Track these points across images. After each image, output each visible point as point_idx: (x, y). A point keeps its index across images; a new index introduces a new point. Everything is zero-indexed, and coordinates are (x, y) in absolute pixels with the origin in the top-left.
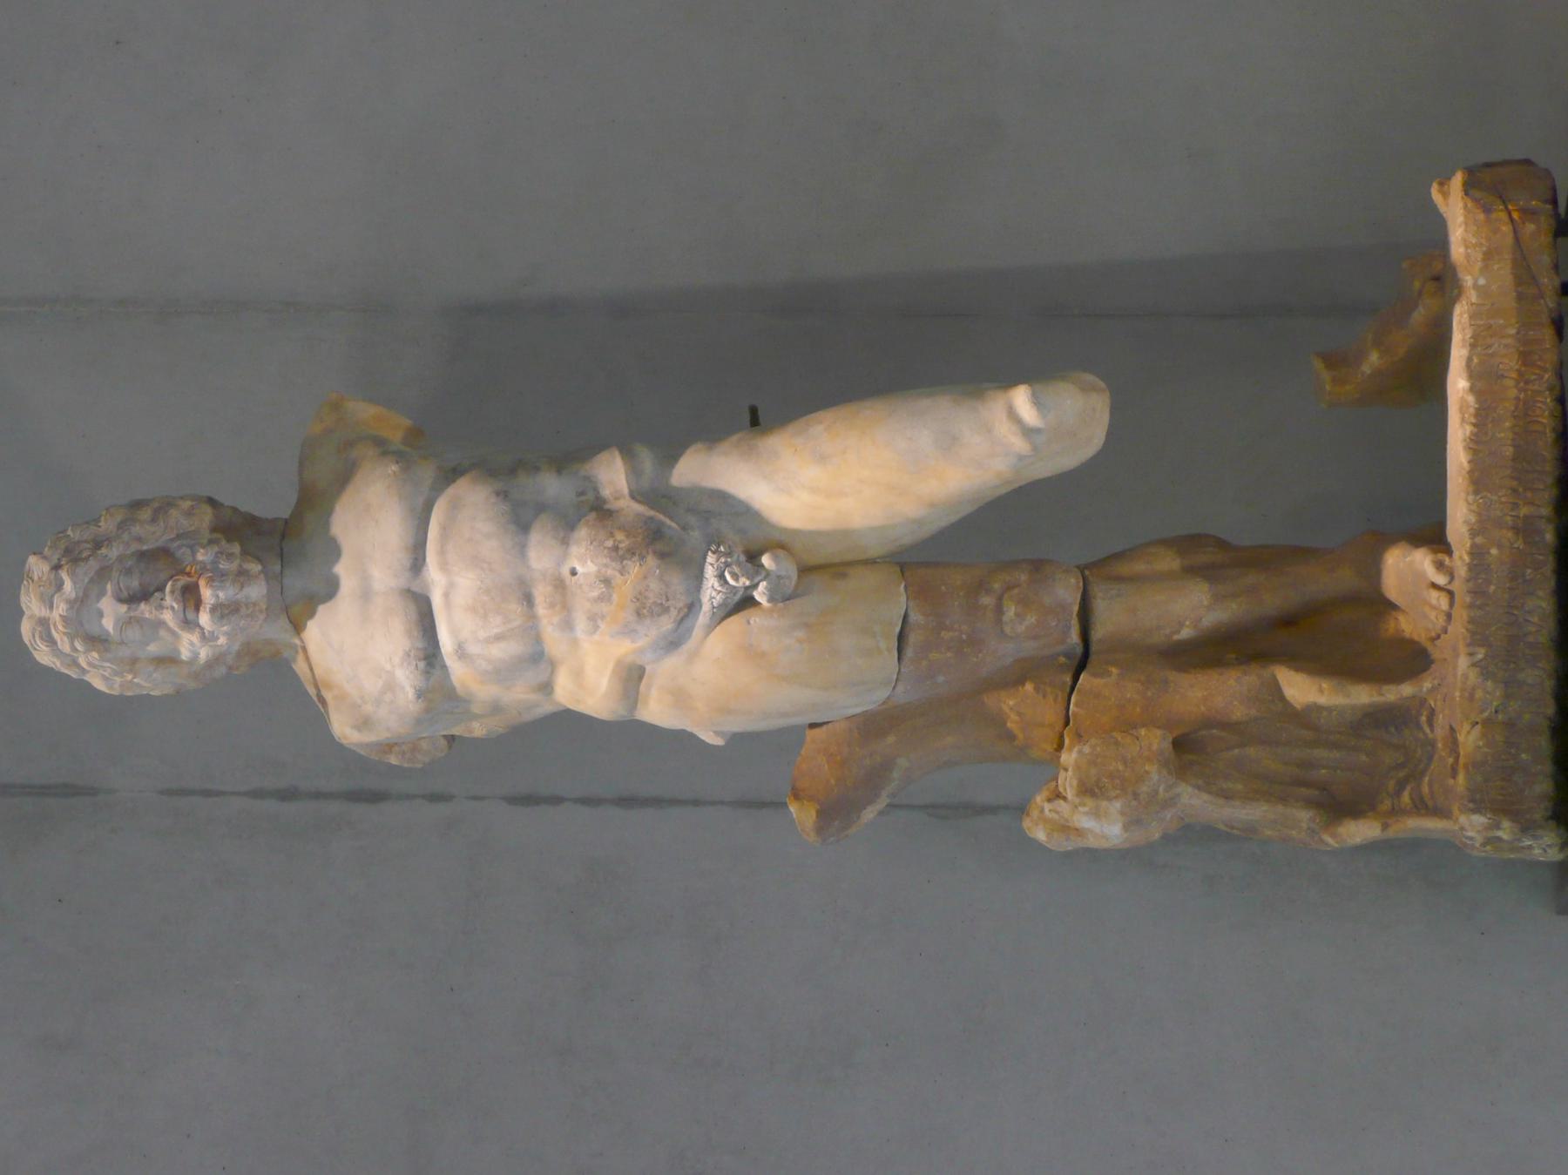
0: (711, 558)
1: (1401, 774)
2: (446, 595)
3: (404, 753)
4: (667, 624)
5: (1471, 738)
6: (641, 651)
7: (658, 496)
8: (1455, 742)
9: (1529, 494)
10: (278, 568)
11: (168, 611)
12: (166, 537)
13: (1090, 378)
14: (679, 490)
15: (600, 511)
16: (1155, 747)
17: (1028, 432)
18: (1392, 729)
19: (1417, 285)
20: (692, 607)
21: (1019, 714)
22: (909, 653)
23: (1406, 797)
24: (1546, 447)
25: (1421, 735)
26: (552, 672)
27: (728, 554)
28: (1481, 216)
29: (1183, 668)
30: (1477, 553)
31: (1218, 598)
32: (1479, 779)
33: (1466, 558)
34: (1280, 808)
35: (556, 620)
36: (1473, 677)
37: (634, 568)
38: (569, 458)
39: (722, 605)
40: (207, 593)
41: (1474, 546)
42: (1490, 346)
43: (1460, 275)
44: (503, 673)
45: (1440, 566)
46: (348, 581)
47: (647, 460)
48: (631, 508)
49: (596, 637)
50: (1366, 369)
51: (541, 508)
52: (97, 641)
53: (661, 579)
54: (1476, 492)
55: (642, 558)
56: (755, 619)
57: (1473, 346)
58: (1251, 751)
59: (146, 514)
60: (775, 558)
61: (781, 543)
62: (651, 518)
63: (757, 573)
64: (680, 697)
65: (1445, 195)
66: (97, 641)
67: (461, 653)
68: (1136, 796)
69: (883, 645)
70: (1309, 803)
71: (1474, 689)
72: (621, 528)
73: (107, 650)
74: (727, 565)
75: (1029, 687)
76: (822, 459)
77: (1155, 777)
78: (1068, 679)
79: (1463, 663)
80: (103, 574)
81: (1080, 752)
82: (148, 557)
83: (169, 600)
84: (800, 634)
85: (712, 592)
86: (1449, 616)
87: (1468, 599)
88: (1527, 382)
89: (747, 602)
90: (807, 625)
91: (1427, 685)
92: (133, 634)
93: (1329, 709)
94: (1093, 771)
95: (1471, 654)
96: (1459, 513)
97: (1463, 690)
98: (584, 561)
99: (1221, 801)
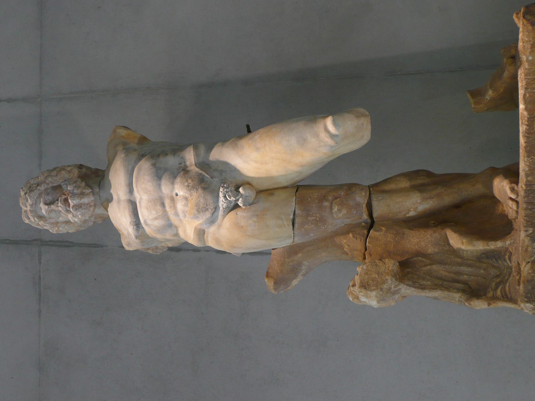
0: (221, 190)
1: (498, 280)
2: (140, 202)
3: (153, 250)
5: (526, 269)
6: (200, 224)
7: (204, 165)
8: (520, 269)
10: (98, 190)
11: (60, 207)
12: (61, 181)
13: (362, 110)
14: (212, 161)
15: (185, 170)
16: (390, 268)
17: (332, 136)
18: (494, 260)
19: (505, 60)
20: (216, 208)
21: (348, 245)
22: (296, 226)
23: (499, 292)
25: (506, 264)
26: (177, 230)
27: (227, 188)
28: (530, 28)
29: (410, 228)
30: (528, 184)
32: (530, 288)
33: (524, 186)
34: (446, 293)
35: (173, 212)
36: (527, 241)
37: (195, 194)
38: (177, 149)
39: (227, 207)
40: (70, 201)
41: (527, 181)
43: (521, 56)
44: (160, 230)
45: (513, 190)
46: (115, 197)
47: (202, 149)
48: (194, 169)
49: (186, 219)
50: (488, 97)
51: (166, 170)
52: (41, 217)
54: (528, 156)
55: (197, 189)
56: (239, 213)
57: (526, 89)
58: (434, 267)
60: (244, 189)
61: (247, 183)
62: (201, 174)
63: (238, 195)
64: (218, 241)
65: (519, 19)
66: (41, 217)
67: (145, 221)
68: (381, 289)
69: (285, 223)
70: (458, 290)
71: (528, 246)
72: (190, 178)
73: (46, 220)
74: (227, 192)
75: (351, 235)
76: (258, 149)
77: (390, 281)
79: (523, 234)
80: (40, 195)
81: (362, 268)
83: (60, 204)
84: (255, 219)
85: (222, 203)
86: (517, 212)
87: (525, 206)
89: (236, 206)
90: (257, 215)
91: (508, 242)
92: (53, 215)
93: (466, 251)
95: (526, 231)
96: (523, 166)
97: (522, 247)
98: (180, 190)
99: (420, 290)
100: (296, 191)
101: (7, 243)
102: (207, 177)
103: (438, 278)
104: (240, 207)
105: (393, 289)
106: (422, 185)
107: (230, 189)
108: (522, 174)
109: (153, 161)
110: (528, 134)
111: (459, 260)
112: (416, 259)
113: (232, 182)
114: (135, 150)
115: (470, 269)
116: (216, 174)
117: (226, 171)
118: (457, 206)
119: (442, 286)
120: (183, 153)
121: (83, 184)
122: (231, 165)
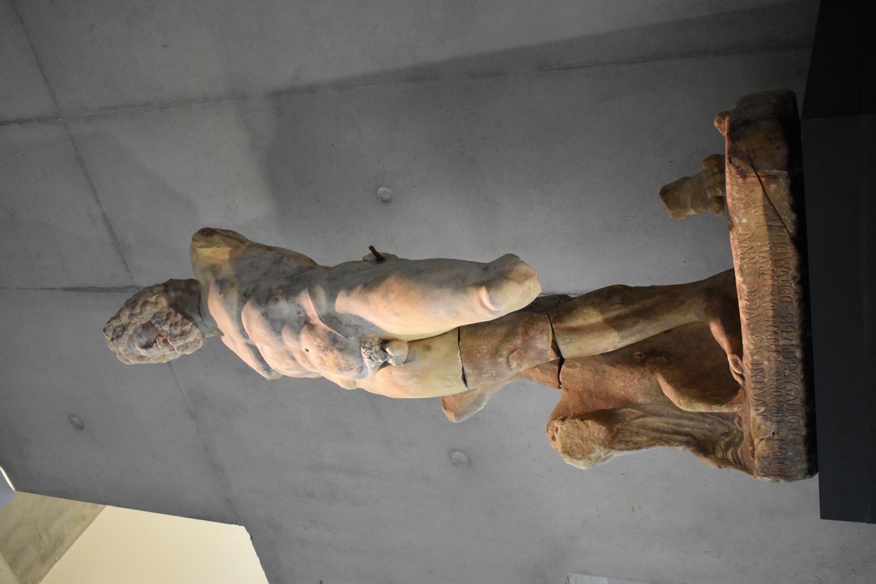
0: (363, 350)
4: (354, 373)
7: (332, 319)
9: (785, 334)
10: (200, 319)
15: (307, 323)
24: (794, 309)
27: (370, 349)
28: (740, 180)
30: (756, 365)
31: (623, 338)
32: (766, 463)
36: (759, 419)
37: (330, 355)
41: (753, 360)
42: (753, 258)
51: (283, 323)
54: (752, 334)
55: (332, 351)
57: (742, 259)
59: (138, 310)
60: (392, 350)
62: (330, 332)
63: (386, 357)
66: (141, 358)
68: (589, 459)
70: (681, 443)
76: (397, 314)
77: (598, 451)
78: (556, 368)
82: (147, 326)
84: (415, 380)
88: (779, 277)
90: (416, 376)
94: (568, 441)
97: (754, 424)
100: (459, 340)
103: (657, 430)
105: (603, 457)
106: (619, 318)
108: (746, 351)
110: (750, 310)
111: (677, 412)
112: (624, 410)
114: (233, 285)
115: (692, 423)
116: (350, 330)
118: (666, 332)
119: (660, 439)
121: (180, 316)
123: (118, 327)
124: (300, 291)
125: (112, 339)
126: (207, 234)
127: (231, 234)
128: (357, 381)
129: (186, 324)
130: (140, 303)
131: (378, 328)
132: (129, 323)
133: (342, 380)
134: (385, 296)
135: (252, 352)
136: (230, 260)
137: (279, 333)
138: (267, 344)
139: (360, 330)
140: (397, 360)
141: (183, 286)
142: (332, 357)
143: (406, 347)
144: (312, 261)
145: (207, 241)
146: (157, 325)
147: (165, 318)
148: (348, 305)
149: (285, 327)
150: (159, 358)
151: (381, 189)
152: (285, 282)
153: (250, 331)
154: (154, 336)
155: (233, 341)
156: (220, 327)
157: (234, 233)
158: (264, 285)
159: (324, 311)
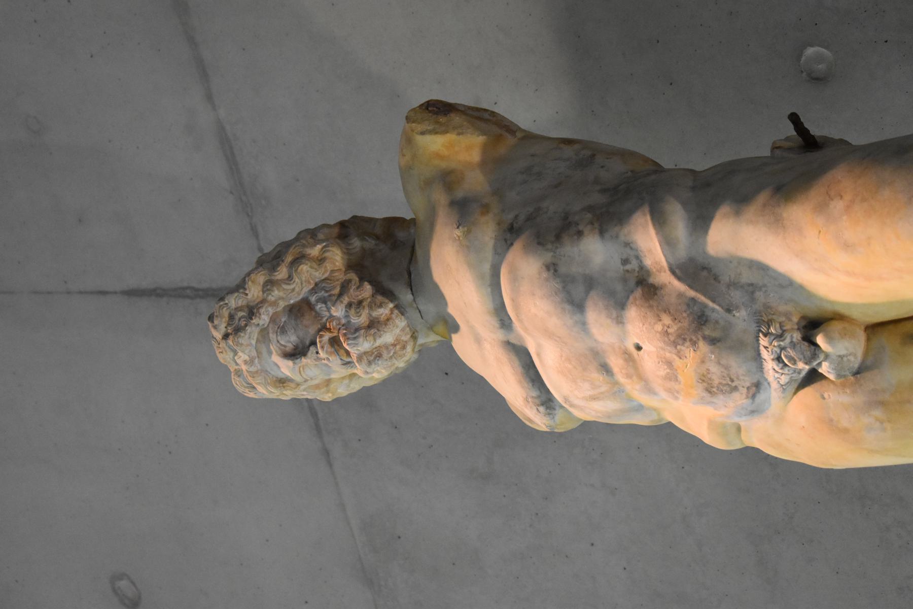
0: (764, 341)
2: (538, 355)
4: (740, 399)
7: (697, 271)
12: (306, 289)
14: (718, 260)
15: (643, 286)
20: (757, 386)
27: (780, 337)
37: (690, 354)
47: (680, 226)
51: (590, 283)
53: (719, 363)
55: (694, 343)
59: (282, 272)
60: (829, 339)
62: (693, 300)
63: (814, 356)
66: (282, 382)
72: (666, 310)
74: (783, 349)
76: (847, 247)
82: (300, 310)
84: (878, 413)
90: (882, 404)
101: (188, 297)
102: (713, 310)
104: (822, 377)
107: (788, 340)
109: (548, 257)
113: (788, 315)
114: (485, 209)
116: (736, 296)
117: (765, 286)
120: (625, 230)
121: (368, 289)
122: (775, 271)
123: (238, 309)
124: (631, 212)
125: (226, 336)
126: (438, 111)
127: (486, 116)
128: (743, 422)
129: (380, 306)
130: (289, 259)
131: (801, 288)
132: (263, 301)
133: (713, 425)
134: (821, 208)
135: (517, 363)
136: (483, 164)
137: (578, 306)
138: (550, 335)
139: (759, 295)
140: (839, 362)
141: (378, 230)
142: (692, 360)
143: (862, 336)
144: (656, 164)
145: (437, 122)
146: (319, 306)
147: (337, 291)
148: (735, 237)
149: (593, 294)
150: (317, 387)
151: (810, 51)
152: (597, 199)
153: (517, 308)
154: (312, 330)
155: (478, 340)
156: (451, 310)
157: (493, 113)
158: (553, 207)
159: (682, 252)
